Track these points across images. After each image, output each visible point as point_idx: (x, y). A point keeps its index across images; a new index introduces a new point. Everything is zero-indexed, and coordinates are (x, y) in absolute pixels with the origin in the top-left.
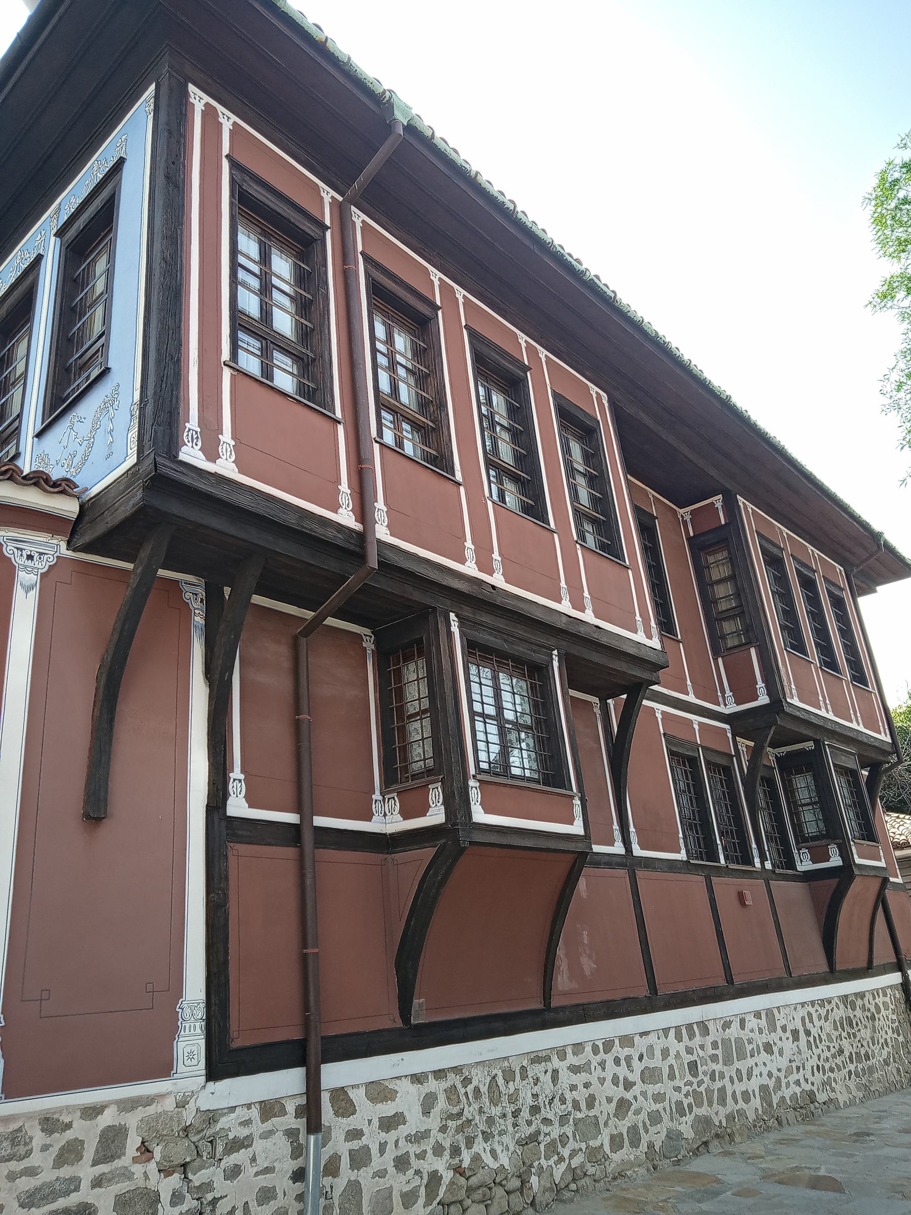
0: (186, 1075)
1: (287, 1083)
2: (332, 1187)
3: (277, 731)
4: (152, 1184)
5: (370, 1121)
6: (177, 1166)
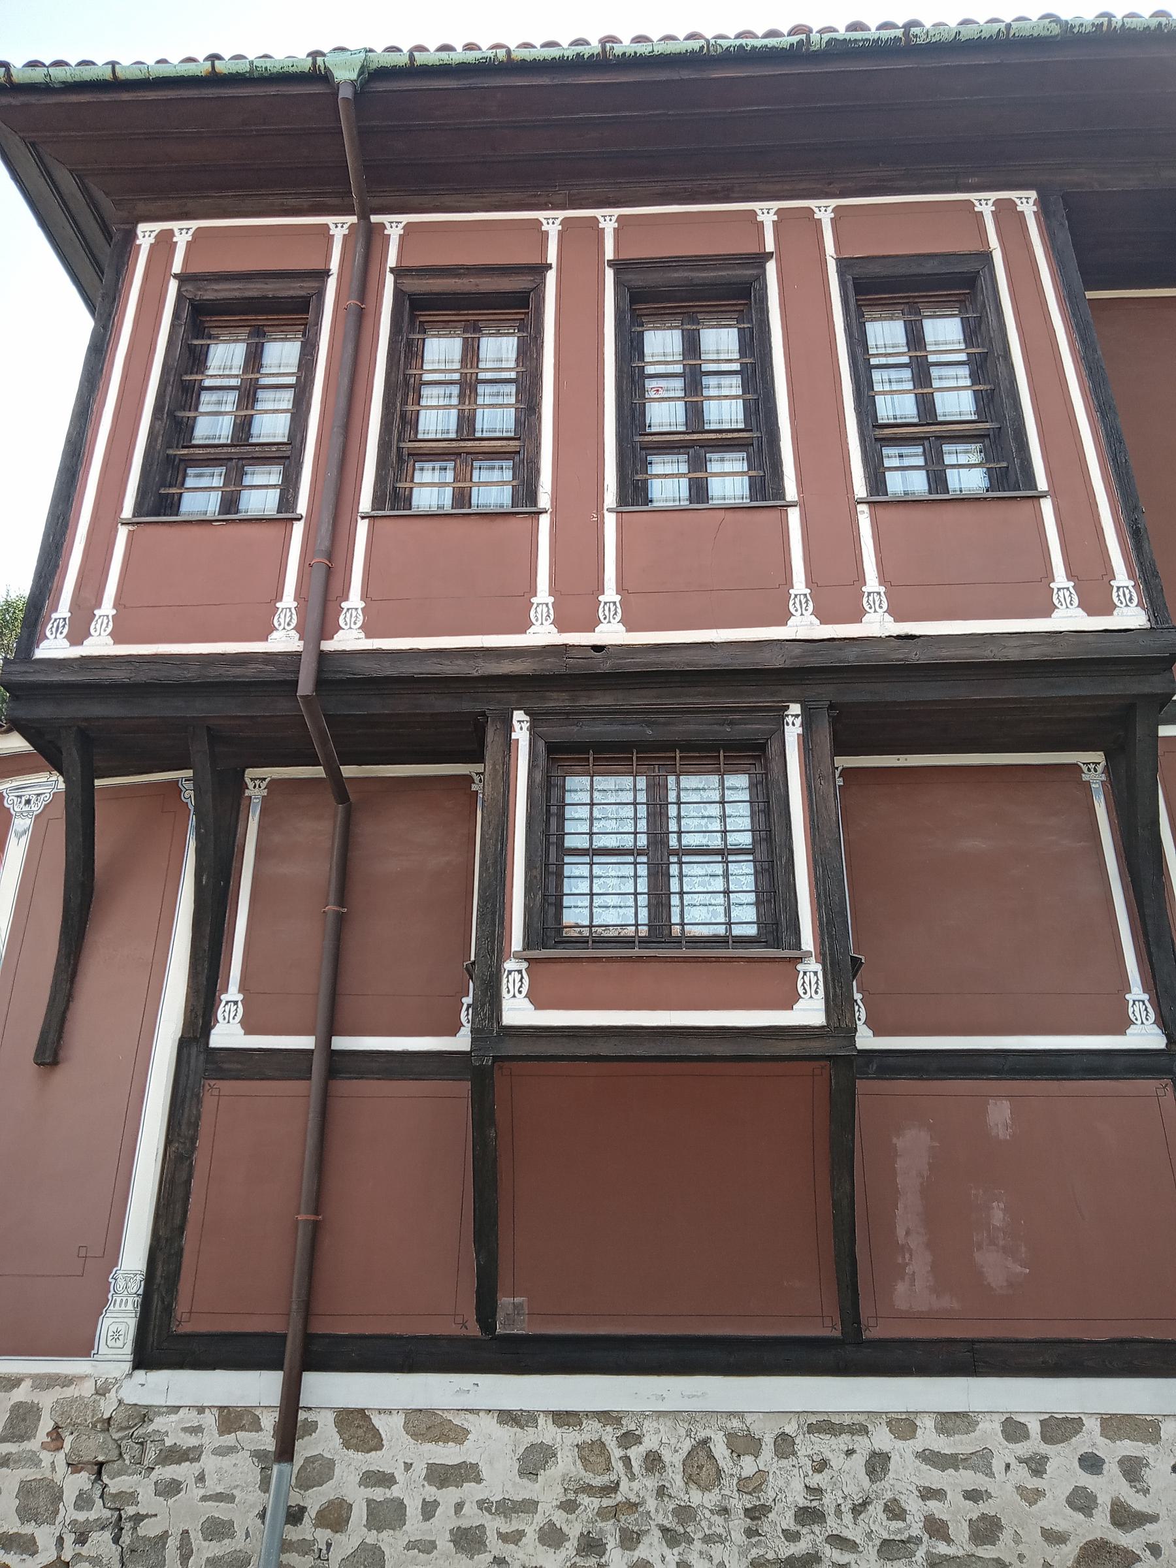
0: (109, 1357)
1: (259, 1388)
2: (329, 1545)
3: (306, 936)
4: (58, 1478)
5: (408, 1466)
6: (88, 1463)
